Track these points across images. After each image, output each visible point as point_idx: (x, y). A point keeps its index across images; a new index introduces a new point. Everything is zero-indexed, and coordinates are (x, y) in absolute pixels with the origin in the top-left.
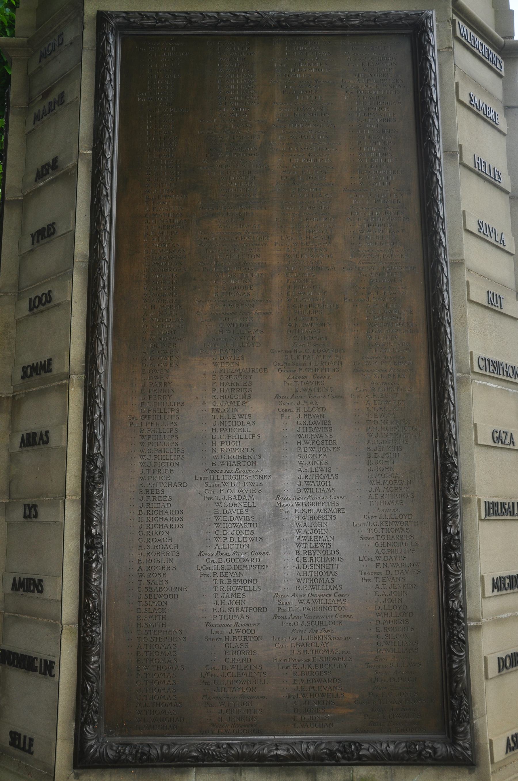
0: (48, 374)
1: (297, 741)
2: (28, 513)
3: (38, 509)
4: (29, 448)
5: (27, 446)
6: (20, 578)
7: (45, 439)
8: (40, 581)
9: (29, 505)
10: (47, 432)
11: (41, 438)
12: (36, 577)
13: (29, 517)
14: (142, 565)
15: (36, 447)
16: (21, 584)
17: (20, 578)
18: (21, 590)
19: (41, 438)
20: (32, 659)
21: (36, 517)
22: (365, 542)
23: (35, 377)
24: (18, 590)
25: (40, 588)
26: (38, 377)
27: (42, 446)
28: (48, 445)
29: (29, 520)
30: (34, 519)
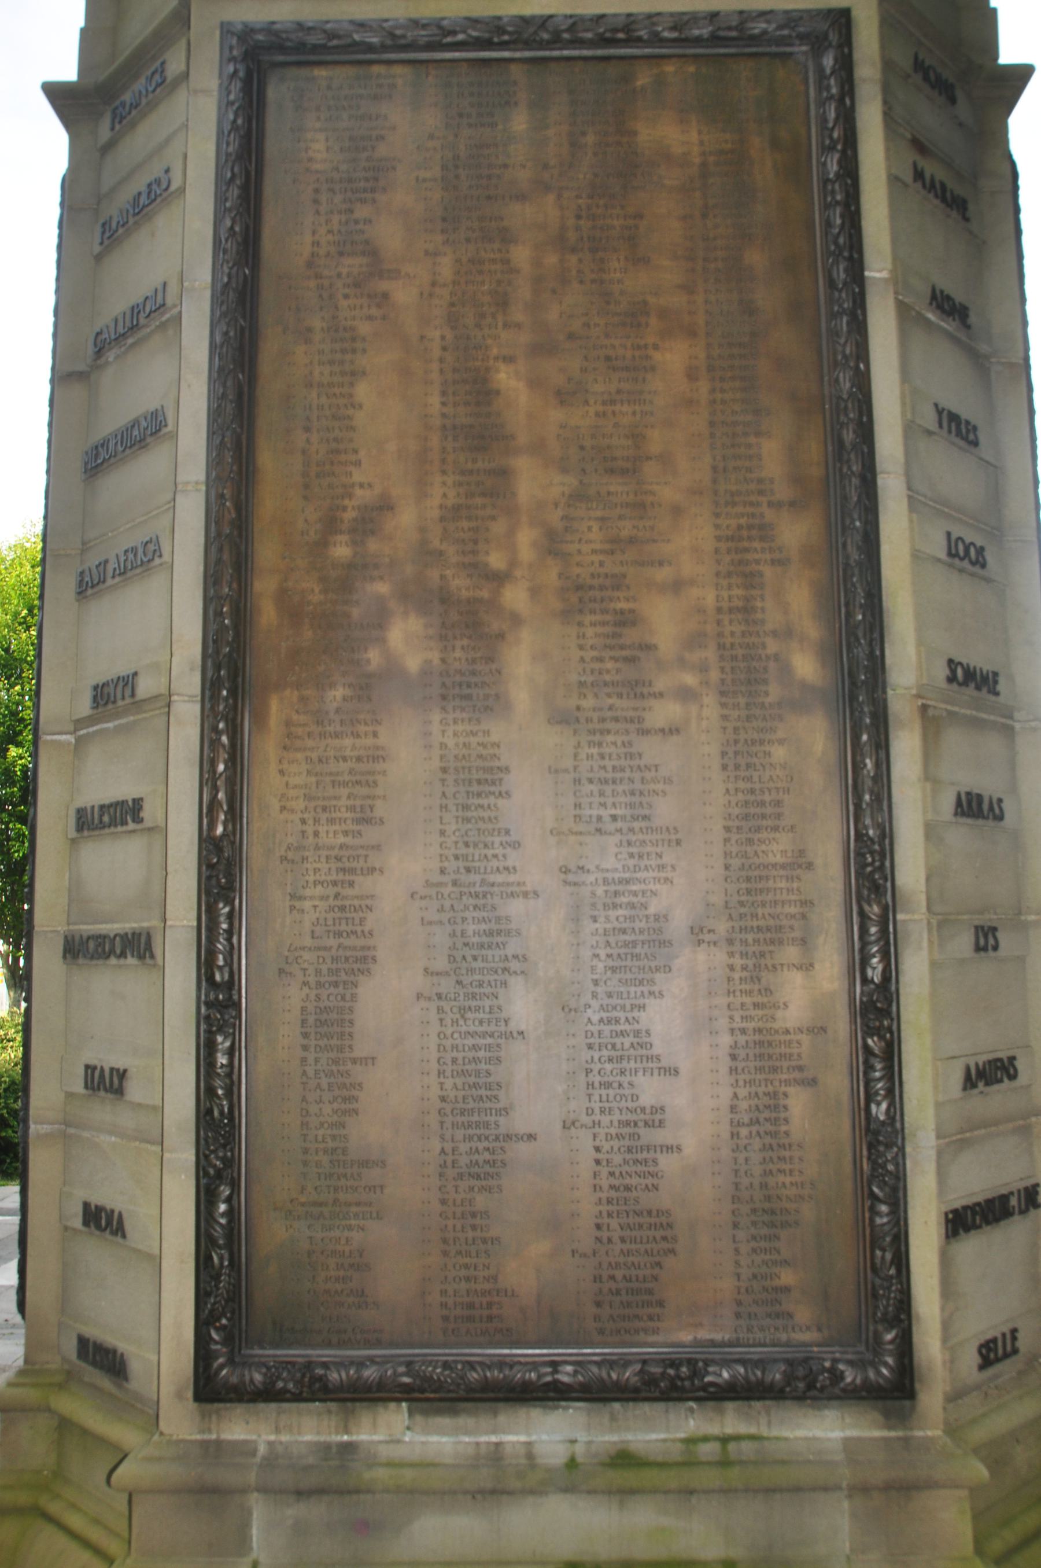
0: (992, 698)
1: (487, 1361)
2: (982, 942)
3: (999, 935)
4: (969, 821)
5: (968, 816)
6: (977, 1065)
7: (997, 811)
8: (1012, 1059)
9: (982, 927)
10: (1000, 801)
11: (991, 808)
12: (1003, 1055)
13: (985, 949)
14: (307, 1068)
15: (980, 822)
16: (981, 1074)
17: (977, 1065)
18: (981, 1085)
19: (991, 808)
20: (1004, 1199)
21: (995, 948)
22: (435, 979)
23: (970, 690)
24: (974, 1086)
25: (1012, 1071)
26: (975, 693)
27: (991, 823)
28: (1002, 823)
29: (982, 954)
30: (991, 953)
